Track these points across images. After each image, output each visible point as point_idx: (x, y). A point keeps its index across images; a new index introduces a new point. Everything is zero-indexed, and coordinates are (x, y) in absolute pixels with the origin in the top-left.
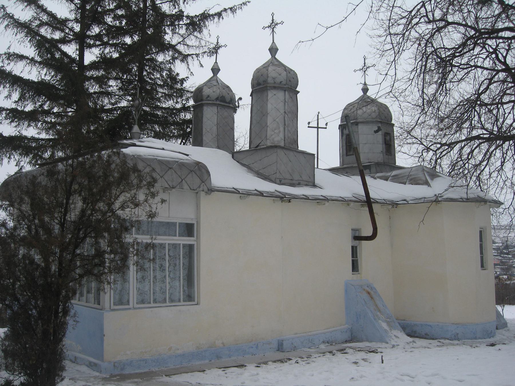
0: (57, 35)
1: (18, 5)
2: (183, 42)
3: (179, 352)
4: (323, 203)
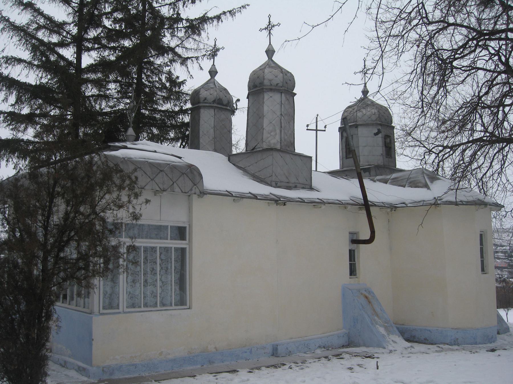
0: (55, 39)
1: (14, 9)
2: (181, 45)
3: (170, 357)
4: (319, 206)
